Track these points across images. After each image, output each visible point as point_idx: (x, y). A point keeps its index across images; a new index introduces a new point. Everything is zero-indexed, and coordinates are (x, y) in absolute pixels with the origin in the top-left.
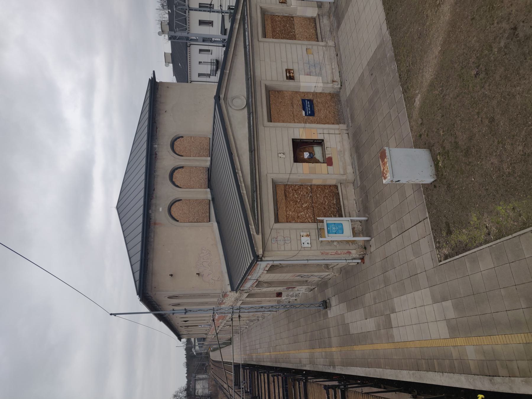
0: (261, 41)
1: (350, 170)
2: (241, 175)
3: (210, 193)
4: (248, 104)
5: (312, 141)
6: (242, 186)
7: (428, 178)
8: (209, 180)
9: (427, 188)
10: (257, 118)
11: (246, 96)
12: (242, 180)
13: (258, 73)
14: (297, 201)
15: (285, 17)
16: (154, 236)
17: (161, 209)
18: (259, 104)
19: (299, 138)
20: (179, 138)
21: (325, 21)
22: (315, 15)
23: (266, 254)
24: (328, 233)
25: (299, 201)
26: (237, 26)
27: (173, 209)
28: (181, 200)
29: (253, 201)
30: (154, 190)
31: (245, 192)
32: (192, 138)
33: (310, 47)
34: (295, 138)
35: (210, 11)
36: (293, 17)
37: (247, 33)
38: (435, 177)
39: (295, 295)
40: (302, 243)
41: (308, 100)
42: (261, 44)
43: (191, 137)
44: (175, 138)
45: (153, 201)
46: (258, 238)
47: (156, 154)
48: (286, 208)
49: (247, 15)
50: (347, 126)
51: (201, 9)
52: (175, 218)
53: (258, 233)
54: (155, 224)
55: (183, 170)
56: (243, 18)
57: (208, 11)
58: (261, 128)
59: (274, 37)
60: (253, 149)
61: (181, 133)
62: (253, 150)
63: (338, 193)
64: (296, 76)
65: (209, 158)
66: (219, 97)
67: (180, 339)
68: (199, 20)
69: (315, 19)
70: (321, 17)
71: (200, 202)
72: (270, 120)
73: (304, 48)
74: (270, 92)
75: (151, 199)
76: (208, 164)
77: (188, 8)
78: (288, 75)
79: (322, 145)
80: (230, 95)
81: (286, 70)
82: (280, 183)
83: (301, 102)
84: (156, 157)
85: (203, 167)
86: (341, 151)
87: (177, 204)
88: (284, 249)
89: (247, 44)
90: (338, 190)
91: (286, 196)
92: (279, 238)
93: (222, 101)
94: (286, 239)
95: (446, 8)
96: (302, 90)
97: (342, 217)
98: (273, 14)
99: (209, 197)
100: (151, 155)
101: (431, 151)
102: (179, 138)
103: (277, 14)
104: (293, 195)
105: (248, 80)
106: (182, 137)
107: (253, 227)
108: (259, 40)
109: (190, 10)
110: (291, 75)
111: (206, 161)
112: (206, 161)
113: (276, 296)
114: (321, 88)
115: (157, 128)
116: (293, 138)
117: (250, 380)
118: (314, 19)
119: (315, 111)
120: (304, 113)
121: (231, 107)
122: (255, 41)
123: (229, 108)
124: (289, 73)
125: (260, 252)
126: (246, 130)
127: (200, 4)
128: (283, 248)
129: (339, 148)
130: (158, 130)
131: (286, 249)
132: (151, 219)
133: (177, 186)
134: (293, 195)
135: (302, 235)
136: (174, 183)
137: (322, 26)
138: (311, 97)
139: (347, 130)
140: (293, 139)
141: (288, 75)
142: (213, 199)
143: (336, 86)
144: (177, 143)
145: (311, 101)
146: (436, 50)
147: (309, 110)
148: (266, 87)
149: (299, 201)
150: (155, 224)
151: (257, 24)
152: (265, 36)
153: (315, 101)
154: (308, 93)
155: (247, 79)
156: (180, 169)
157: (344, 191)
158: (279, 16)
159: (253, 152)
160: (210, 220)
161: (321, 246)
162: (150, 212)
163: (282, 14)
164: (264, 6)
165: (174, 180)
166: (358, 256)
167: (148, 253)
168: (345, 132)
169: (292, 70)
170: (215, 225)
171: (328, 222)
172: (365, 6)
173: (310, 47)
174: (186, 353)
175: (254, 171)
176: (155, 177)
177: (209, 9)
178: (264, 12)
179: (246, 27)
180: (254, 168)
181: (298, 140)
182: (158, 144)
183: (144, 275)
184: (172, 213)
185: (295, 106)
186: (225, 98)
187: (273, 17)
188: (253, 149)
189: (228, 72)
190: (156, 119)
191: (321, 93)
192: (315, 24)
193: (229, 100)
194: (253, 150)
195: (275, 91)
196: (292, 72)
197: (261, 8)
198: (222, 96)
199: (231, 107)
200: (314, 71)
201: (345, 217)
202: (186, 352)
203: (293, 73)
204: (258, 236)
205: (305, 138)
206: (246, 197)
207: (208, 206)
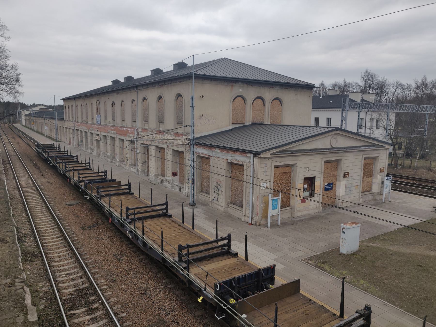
0: (362, 157)
1: (299, 214)
2: (300, 143)
3: (249, 124)
4: (333, 148)
5: (313, 190)
6: (295, 144)
7: (344, 250)
8: (256, 124)
9: (338, 249)
10: (326, 154)
11: (337, 147)
12: (298, 144)
13: (347, 154)
14: (282, 180)
15: (372, 172)
16: (225, 85)
17: (241, 90)
18: (333, 155)
19: (316, 181)
20: (281, 103)
21: (371, 197)
22: (373, 191)
23: (260, 160)
24: (273, 200)
25: (283, 181)
26: (371, 142)
27: (240, 99)
28: (245, 104)
29: (290, 151)
30: (252, 86)
31: (292, 146)
32: (280, 113)
33: (359, 188)
34: (316, 179)
35: (358, 125)
36: (372, 177)
37: (367, 147)
38: (347, 254)
39: (173, 187)
40: (263, 183)
41: (332, 186)
42: (361, 157)
43: (281, 112)
44: (281, 101)
45: (245, 85)
46: (268, 154)
47: (272, 88)
48: (280, 173)
49: (376, 148)
50: (321, 212)
51: (359, 119)
52: (235, 100)
53: (271, 154)
54: (232, 86)
55: (263, 106)
56: (374, 145)
57: (358, 124)
58: (320, 157)
59: (365, 165)
60: (313, 151)
61: (284, 104)
62: (312, 152)
63: (285, 207)
64: (345, 179)
65: (269, 123)
66: (338, 130)
67: (65, 100)
68: (319, 118)
69: (371, 191)
70: (372, 194)
71: (244, 117)
72: (326, 162)
73: (359, 184)
74: (337, 162)
75: (247, 84)
76: (266, 123)
77: (360, 111)
78: (346, 174)
79: (310, 196)
80: (339, 137)
81: (348, 173)
82: (292, 169)
83: (331, 182)
84: (271, 87)
85: (264, 119)
86: (308, 208)
87: (243, 101)
88: (261, 171)
89: (362, 148)
90: (287, 207)
91: (285, 173)
92: (266, 168)
93: (336, 132)
94: (266, 173)
95: (432, 253)
96: (337, 182)
97: (281, 208)
98: (374, 164)
99: (247, 124)
100: (272, 84)
101: (358, 251)
102: (281, 103)
103: (374, 166)
104: (286, 178)
105: (345, 149)
106: (281, 106)
107: (274, 152)
108: (363, 156)
109: (359, 112)
110: (346, 176)
111: (268, 122)
112: (268, 122)
113: (173, 172)
114: (339, 195)
115: (287, 89)
116: (316, 177)
117: (62, 156)
118: (370, 190)
119: (327, 191)
120: (326, 184)
121: (332, 137)
122: (362, 153)
123: (331, 136)
124: (347, 174)
125: (262, 156)
126: (321, 147)
127: (331, 118)
128: (261, 171)
129: (310, 207)
130: (286, 89)
131: (261, 173)
132: (235, 83)
133: (253, 102)
134: (286, 178)
135: (267, 183)
136: (255, 99)
137: (368, 195)
138: (334, 189)
139: (319, 212)
140: (315, 177)
141: (346, 174)
142: (246, 126)
143: (340, 204)
144: (278, 102)
145: (331, 189)
146: (408, 251)
147: (328, 188)
148: (340, 160)
149: (283, 181)
150: (232, 86)
151: (371, 154)
152: (365, 159)
153: (331, 191)
154: (336, 186)
155: (345, 148)
156: (263, 104)
157: (287, 211)
158: (373, 168)
159: (329, 150)
160: (233, 124)
161: (261, 196)
162: (240, 83)
163: (374, 170)
164: (379, 158)
165: (257, 99)
166: (255, 220)
167: (215, 81)
168: (318, 211)
169: (348, 176)
170: (230, 128)
171: (278, 200)
172: (253, 255)
173: (359, 188)
174: (5, 102)
175: (302, 152)
176: (259, 86)
177: (359, 124)
178: (375, 158)
179: (370, 147)
180: (303, 152)
181: (314, 180)
182: (278, 89)
183: (218, 79)
184: (238, 98)
185: (330, 178)
186: (337, 134)
187: (372, 164)
188: (347, 149)
189: (350, 136)
190: (292, 88)
191: (335, 195)
192: (368, 191)
193: (335, 136)
194: (312, 152)
195: (337, 166)
196: (347, 176)
197: (378, 157)
198: (338, 132)
199: (332, 137)
200: (348, 190)
201: (281, 211)
202: (6, 102)
203: (347, 177)
204: (270, 154)
205: (315, 185)
206: (289, 147)
207: (241, 123)
